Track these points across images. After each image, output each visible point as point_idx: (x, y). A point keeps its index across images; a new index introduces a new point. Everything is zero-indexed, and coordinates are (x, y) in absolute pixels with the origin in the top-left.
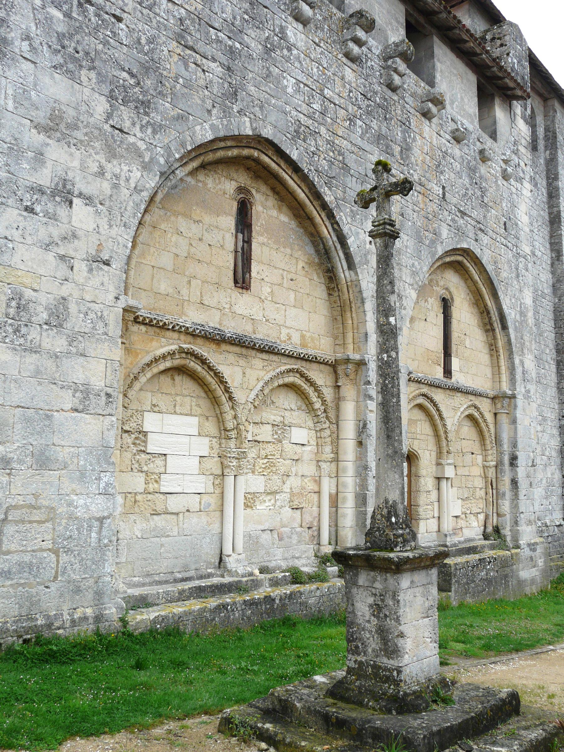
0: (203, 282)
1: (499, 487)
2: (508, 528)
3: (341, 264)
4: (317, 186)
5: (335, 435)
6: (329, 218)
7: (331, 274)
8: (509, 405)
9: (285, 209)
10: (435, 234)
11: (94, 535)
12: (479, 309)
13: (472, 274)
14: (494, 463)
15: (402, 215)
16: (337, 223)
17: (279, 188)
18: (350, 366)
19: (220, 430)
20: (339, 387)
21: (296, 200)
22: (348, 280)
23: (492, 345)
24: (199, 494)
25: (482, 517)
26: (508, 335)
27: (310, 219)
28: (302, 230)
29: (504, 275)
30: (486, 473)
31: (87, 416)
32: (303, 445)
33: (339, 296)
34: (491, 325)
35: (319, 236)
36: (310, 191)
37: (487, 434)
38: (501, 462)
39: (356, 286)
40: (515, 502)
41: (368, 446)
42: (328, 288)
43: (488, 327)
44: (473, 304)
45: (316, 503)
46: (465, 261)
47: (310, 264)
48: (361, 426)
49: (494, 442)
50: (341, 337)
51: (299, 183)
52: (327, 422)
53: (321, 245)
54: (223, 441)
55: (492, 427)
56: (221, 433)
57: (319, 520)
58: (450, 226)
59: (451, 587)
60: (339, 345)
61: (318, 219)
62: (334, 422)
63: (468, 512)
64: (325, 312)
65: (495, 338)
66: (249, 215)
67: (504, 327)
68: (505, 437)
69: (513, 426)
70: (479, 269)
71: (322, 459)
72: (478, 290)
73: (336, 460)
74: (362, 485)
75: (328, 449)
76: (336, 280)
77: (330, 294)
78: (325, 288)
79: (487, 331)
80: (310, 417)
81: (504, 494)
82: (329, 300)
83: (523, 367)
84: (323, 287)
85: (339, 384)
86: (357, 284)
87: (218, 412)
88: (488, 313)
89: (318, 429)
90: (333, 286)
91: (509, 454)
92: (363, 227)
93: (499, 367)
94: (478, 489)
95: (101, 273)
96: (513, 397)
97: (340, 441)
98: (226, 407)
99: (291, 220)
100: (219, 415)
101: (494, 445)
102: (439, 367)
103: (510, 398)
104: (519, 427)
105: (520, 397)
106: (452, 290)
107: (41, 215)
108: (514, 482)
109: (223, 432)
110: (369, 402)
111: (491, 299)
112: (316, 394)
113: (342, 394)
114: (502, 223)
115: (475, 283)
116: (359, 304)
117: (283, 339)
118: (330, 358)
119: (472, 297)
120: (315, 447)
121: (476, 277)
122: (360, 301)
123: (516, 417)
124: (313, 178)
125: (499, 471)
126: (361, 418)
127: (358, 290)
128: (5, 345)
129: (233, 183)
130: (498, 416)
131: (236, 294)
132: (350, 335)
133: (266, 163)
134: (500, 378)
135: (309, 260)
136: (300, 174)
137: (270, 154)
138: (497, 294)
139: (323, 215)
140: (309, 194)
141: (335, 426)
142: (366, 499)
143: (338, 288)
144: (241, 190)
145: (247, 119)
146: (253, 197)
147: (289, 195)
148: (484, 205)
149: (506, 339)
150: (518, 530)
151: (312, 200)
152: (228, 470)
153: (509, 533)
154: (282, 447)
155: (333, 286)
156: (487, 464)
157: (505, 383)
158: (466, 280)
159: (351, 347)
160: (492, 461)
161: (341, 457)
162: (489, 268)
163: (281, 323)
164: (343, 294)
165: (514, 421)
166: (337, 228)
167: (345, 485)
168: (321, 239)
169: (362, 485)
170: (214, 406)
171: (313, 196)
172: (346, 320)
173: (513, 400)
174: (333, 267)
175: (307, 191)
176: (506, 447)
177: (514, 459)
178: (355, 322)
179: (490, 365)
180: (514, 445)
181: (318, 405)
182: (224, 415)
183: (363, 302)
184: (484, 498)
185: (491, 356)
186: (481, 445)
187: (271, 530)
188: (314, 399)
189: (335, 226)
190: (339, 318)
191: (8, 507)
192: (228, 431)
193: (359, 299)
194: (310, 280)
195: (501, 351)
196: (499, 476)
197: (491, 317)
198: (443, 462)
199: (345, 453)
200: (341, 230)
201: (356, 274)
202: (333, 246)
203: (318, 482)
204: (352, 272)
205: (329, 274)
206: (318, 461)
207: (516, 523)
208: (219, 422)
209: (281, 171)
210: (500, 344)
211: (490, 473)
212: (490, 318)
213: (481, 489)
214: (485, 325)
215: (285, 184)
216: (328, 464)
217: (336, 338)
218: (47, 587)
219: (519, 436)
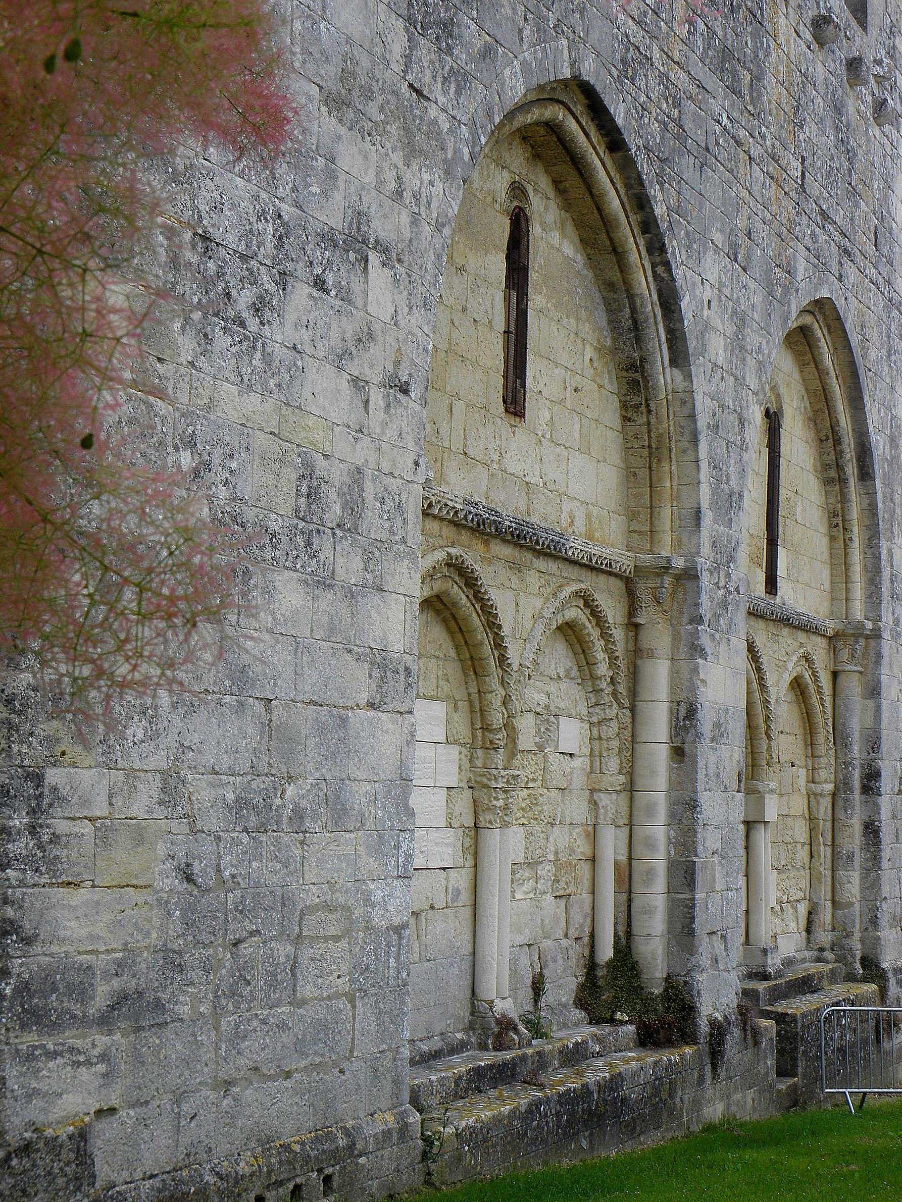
0: (467, 406)
1: (839, 840)
2: (857, 935)
3: (660, 353)
4: (647, 183)
5: (627, 733)
6: (650, 251)
7: (638, 376)
8: (865, 654)
9: (570, 227)
10: (789, 272)
11: (392, 960)
12: (818, 431)
13: (821, 354)
14: (830, 787)
15: (749, 235)
16: (667, 265)
17: (572, 180)
18: (668, 580)
19: (474, 729)
20: (637, 626)
21: (599, 210)
22: (670, 388)
23: (835, 515)
24: (444, 869)
25: (803, 909)
26: (871, 495)
27: (618, 253)
28: (591, 275)
29: (873, 354)
30: (814, 809)
31: (384, 716)
32: (571, 755)
33: (649, 423)
34: (840, 468)
35: (628, 291)
36: (626, 194)
37: (819, 720)
38: (846, 784)
39: (683, 402)
40: (873, 875)
41: (699, 759)
42: (624, 405)
43: (833, 474)
44: (809, 418)
45: (586, 883)
46: (816, 326)
47: (599, 350)
48: (683, 712)
49: (831, 739)
50: (644, 515)
51: (612, 174)
52: (615, 705)
53: (628, 310)
54: (480, 753)
55: (828, 700)
56: (474, 736)
57: (593, 921)
58: (809, 250)
59: (795, 1066)
60: (640, 533)
61: (634, 257)
62: (627, 704)
63: (785, 898)
64: (615, 456)
65: (844, 499)
66: (523, 247)
67: (866, 474)
68: (856, 725)
69: (871, 703)
70: (834, 343)
71: (603, 786)
72: (824, 389)
73: (631, 789)
74: (684, 845)
75: (613, 764)
76: (646, 388)
77: (625, 419)
78: (617, 404)
79: (827, 482)
80: (582, 693)
81: (850, 857)
82: (623, 432)
83: (892, 566)
84: (614, 403)
85: (639, 620)
86: (687, 399)
87: (473, 690)
88: (837, 441)
89: (595, 719)
90: (636, 400)
91: (862, 766)
92: (701, 269)
93: (847, 565)
94: (799, 846)
95: (400, 410)
96: (877, 635)
97: (640, 748)
98: (494, 682)
99: (577, 252)
100: (475, 697)
101: (831, 745)
102: (758, 570)
103: (867, 637)
104: (885, 704)
105: (886, 635)
106: (783, 390)
107: (333, 293)
108: (872, 830)
109: (479, 733)
110: (700, 661)
111: (847, 408)
112: (603, 643)
113: (645, 643)
114: (873, 229)
115: (821, 373)
116: (686, 444)
117: (564, 524)
118: (625, 561)
119: (808, 405)
120: (587, 760)
121: (828, 362)
122: (687, 436)
123: (879, 682)
124: (642, 166)
125: (840, 803)
126: (682, 696)
127: (686, 411)
128: (295, 575)
129: (505, 173)
130: (842, 679)
131: (501, 422)
132: (666, 513)
133: (571, 133)
134: (848, 590)
135: (599, 341)
136: (620, 154)
137: (578, 113)
138: (862, 398)
139: (641, 243)
140: (625, 199)
141: (628, 712)
142: (693, 874)
143: (648, 406)
144: (517, 190)
145: (565, 42)
146: (530, 205)
147: (588, 199)
148: (853, 193)
149: (866, 502)
150: (879, 938)
151: (628, 210)
152: (489, 816)
153: (859, 947)
154: (545, 761)
155: (636, 400)
156: (817, 788)
157: (858, 603)
158: (802, 365)
159: (667, 538)
160: (826, 781)
161: (640, 783)
162: (855, 339)
163: (562, 490)
164: (659, 422)
165: (874, 691)
166: (665, 275)
167: (650, 844)
168: (631, 297)
169: (684, 845)
170: (466, 675)
171: (630, 202)
172: (660, 479)
173: (872, 643)
174: (643, 360)
175: (622, 192)
176: (857, 750)
177: (871, 777)
178: (675, 483)
179: (828, 562)
180: (874, 744)
181: (603, 669)
182: (489, 696)
183: (695, 440)
184: (807, 867)
185: (832, 539)
186: (806, 745)
187: (529, 945)
188: (601, 655)
189: (660, 270)
190: (643, 473)
191: (302, 910)
192: (491, 731)
193: (687, 433)
194: (600, 387)
195: (856, 529)
196: (840, 814)
197: (842, 452)
198: (760, 786)
199: (653, 773)
200: (673, 280)
201: (689, 377)
202: (651, 314)
203: (593, 837)
204: (677, 373)
205: (632, 375)
206: (593, 791)
207: (874, 921)
208: (472, 712)
209: (591, 150)
210: (855, 513)
211: (822, 809)
212: (839, 454)
213: (803, 844)
214: (825, 467)
215: (591, 176)
216: (614, 796)
217: (632, 516)
218: (342, 1071)
219: (883, 726)
